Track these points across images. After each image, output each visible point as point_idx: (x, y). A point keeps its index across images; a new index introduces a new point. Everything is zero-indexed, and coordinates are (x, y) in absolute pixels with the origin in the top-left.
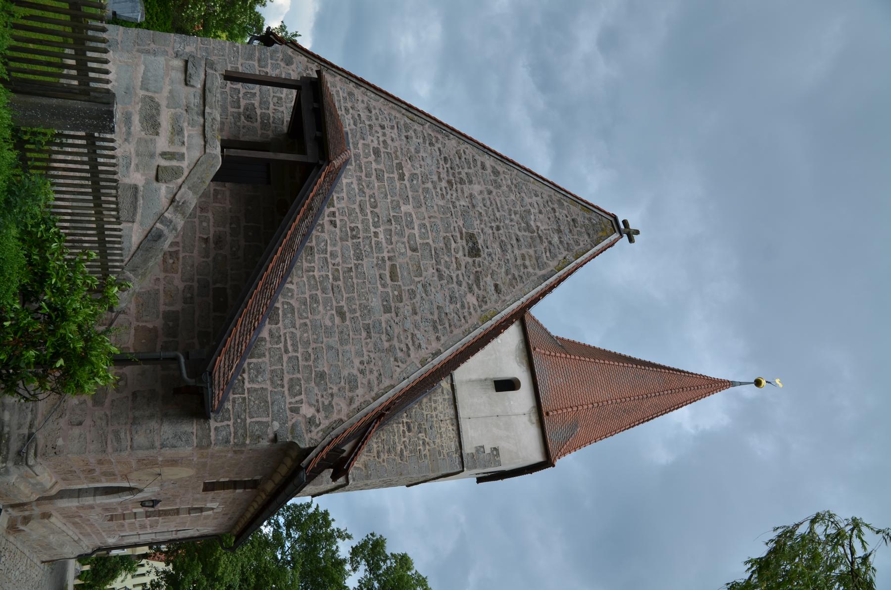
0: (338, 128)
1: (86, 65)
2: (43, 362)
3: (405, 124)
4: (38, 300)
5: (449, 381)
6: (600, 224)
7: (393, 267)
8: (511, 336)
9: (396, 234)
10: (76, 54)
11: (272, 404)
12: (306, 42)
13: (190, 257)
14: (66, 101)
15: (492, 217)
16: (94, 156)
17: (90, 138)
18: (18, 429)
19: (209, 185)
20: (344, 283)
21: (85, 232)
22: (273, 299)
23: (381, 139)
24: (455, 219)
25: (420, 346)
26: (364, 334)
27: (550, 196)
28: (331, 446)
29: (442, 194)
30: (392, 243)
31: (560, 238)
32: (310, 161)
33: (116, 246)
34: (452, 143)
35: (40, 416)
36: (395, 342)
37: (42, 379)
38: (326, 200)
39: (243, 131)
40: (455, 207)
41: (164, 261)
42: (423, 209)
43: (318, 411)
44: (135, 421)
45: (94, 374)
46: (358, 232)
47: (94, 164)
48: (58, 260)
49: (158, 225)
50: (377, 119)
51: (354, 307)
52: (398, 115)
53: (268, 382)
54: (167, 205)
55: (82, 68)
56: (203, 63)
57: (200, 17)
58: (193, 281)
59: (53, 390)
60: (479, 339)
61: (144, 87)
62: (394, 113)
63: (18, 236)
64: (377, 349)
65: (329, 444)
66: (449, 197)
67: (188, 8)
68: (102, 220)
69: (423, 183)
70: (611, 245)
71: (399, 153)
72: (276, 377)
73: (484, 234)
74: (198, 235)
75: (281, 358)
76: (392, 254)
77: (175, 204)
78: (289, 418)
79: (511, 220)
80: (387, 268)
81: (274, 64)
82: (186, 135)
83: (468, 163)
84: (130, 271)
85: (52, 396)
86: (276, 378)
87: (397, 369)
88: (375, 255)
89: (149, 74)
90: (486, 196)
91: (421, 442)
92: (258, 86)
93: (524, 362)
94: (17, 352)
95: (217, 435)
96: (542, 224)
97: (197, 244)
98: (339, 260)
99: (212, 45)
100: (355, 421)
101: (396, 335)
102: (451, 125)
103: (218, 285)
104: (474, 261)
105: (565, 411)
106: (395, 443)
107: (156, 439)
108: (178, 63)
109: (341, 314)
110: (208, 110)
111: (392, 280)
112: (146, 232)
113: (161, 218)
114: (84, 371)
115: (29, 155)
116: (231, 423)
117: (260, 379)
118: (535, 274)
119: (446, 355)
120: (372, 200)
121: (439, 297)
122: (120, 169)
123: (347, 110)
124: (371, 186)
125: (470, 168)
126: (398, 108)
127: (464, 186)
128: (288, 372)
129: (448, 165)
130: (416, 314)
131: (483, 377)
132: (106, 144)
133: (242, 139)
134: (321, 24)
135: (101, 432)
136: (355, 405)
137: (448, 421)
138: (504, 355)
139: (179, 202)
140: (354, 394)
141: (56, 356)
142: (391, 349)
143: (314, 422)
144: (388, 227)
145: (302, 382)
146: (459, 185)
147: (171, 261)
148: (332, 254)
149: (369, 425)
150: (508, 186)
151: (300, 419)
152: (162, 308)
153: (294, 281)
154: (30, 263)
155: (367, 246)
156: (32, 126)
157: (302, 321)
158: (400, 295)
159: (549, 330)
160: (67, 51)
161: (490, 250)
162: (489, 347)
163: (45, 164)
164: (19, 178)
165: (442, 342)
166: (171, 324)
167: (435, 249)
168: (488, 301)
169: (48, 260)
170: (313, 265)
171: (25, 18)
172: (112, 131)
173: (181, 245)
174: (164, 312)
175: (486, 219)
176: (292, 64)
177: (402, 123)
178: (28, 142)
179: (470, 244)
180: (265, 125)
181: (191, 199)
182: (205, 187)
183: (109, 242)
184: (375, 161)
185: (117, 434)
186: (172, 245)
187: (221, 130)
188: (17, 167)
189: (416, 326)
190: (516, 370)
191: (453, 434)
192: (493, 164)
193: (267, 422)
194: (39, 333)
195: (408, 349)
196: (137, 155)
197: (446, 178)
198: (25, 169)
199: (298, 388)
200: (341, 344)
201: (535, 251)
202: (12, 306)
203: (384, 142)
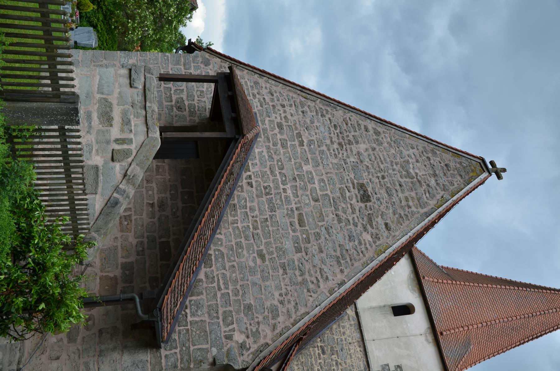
0: (249, 109)
1: (57, 75)
2: (29, 307)
3: (301, 102)
4: (25, 258)
5: (354, 309)
6: (470, 166)
7: (300, 215)
8: (403, 267)
9: (301, 188)
10: (49, 68)
11: (210, 334)
12: (218, 47)
13: (140, 218)
14: (43, 103)
15: (377, 169)
16: (65, 144)
17: (62, 130)
18: (9, 366)
19: (152, 162)
20: (262, 230)
21: (59, 203)
22: (206, 247)
23: (283, 115)
24: (347, 173)
25: (327, 278)
26: (281, 271)
27: (424, 148)
28: (260, 367)
29: (335, 154)
30: (298, 196)
31: (436, 181)
32: (229, 136)
33: (84, 212)
34: (339, 113)
35: (26, 354)
36: (307, 276)
37: (28, 322)
38: (243, 166)
39: (175, 119)
40: (346, 163)
41: (121, 223)
42: (321, 167)
43: (248, 337)
44: (101, 354)
45: (68, 314)
46: (270, 190)
47: (65, 150)
48: (41, 225)
49: (115, 195)
50: (278, 100)
51: (271, 249)
52: (294, 96)
53: (206, 315)
54: (121, 179)
55: (54, 78)
56: (143, 70)
57: (138, 40)
58: (143, 237)
59: (36, 330)
60: (376, 269)
61: (100, 92)
62: (291, 94)
63: (10, 209)
64: (293, 283)
65: (258, 365)
66: (340, 156)
67: (129, 34)
68: (72, 192)
69: (319, 146)
70: (482, 183)
71: (298, 125)
72: (213, 310)
73: (372, 183)
74: (145, 201)
75: (215, 295)
76: (299, 205)
77: (127, 177)
78: (225, 344)
79: (394, 170)
80: (296, 217)
81: (196, 66)
82: (133, 125)
83: (354, 127)
84: (95, 232)
85: (36, 336)
86: (212, 311)
87: (310, 298)
88: (285, 207)
89: (103, 82)
90: (371, 152)
91: (334, 363)
92: (185, 83)
93: (416, 289)
94: (9, 300)
95: (167, 362)
96: (419, 170)
97: (145, 208)
98: (257, 213)
99: (149, 57)
100: (279, 344)
101: (307, 271)
102: (337, 99)
103: (163, 240)
104: (366, 206)
105: (457, 330)
106: (312, 365)
107: (118, 367)
108: (125, 72)
109: (262, 256)
110: (148, 104)
111: (300, 226)
112: (106, 201)
113: (117, 189)
114: (60, 312)
115: (17, 147)
116: (178, 351)
117: (199, 313)
118: (418, 212)
119: (349, 284)
120: (280, 163)
121: (340, 236)
122: (85, 154)
123: (254, 96)
124: (278, 152)
125: (355, 131)
126: (294, 90)
127: (352, 146)
128: (222, 306)
129: (338, 131)
130: (322, 252)
131: (382, 304)
132: (74, 134)
133: (175, 125)
134: (228, 38)
135: (74, 364)
136: (278, 330)
137: (356, 344)
138: (398, 283)
139: (130, 176)
140: (276, 321)
141: (39, 302)
142: (304, 282)
143: (245, 346)
144: (294, 184)
145: (234, 314)
146: (348, 146)
147: (126, 223)
148: (250, 209)
149: (290, 348)
150: (388, 143)
151: (233, 344)
152: (121, 260)
153: (223, 232)
154: (19, 229)
155: (278, 201)
156: (18, 125)
157: (230, 264)
158: (308, 238)
159: (434, 261)
160: (43, 74)
161: (379, 196)
162: (384, 278)
163: (29, 153)
164: (10, 165)
165: (345, 274)
166: (127, 272)
167: (333, 198)
168: (381, 238)
169: (32, 226)
170: (236, 218)
171: (12, 44)
172: (78, 123)
173: (133, 210)
174: (122, 264)
175: (373, 170)
176: (209, 65)
177: (298, 101)
178: (16, 137)
179: (362, 192)
180: (192, 113)
181: (138, 172)
182: (149, 163)
183: (78, 210)
184: (279, 133)
185: (87, 365)
186: (125, 210)
187: (159, 119)
188: (8, 157)
189: (323, 262)
190: (410, 297)
191: (361, 355)
192: (374, 126)
193: (207, 349)
194: (26, 284)
195: (318, 281)
196: (97, 143)
197: (337, 141)
198: (14, 157)
199: (230, 318)
200: (263, 281)
201: (417, 194)
202: (5, 264)
203: (286, 117)
